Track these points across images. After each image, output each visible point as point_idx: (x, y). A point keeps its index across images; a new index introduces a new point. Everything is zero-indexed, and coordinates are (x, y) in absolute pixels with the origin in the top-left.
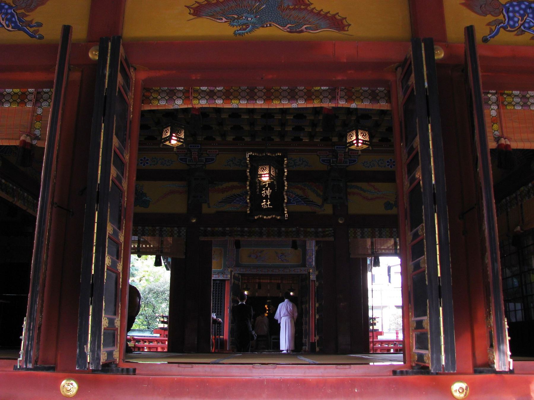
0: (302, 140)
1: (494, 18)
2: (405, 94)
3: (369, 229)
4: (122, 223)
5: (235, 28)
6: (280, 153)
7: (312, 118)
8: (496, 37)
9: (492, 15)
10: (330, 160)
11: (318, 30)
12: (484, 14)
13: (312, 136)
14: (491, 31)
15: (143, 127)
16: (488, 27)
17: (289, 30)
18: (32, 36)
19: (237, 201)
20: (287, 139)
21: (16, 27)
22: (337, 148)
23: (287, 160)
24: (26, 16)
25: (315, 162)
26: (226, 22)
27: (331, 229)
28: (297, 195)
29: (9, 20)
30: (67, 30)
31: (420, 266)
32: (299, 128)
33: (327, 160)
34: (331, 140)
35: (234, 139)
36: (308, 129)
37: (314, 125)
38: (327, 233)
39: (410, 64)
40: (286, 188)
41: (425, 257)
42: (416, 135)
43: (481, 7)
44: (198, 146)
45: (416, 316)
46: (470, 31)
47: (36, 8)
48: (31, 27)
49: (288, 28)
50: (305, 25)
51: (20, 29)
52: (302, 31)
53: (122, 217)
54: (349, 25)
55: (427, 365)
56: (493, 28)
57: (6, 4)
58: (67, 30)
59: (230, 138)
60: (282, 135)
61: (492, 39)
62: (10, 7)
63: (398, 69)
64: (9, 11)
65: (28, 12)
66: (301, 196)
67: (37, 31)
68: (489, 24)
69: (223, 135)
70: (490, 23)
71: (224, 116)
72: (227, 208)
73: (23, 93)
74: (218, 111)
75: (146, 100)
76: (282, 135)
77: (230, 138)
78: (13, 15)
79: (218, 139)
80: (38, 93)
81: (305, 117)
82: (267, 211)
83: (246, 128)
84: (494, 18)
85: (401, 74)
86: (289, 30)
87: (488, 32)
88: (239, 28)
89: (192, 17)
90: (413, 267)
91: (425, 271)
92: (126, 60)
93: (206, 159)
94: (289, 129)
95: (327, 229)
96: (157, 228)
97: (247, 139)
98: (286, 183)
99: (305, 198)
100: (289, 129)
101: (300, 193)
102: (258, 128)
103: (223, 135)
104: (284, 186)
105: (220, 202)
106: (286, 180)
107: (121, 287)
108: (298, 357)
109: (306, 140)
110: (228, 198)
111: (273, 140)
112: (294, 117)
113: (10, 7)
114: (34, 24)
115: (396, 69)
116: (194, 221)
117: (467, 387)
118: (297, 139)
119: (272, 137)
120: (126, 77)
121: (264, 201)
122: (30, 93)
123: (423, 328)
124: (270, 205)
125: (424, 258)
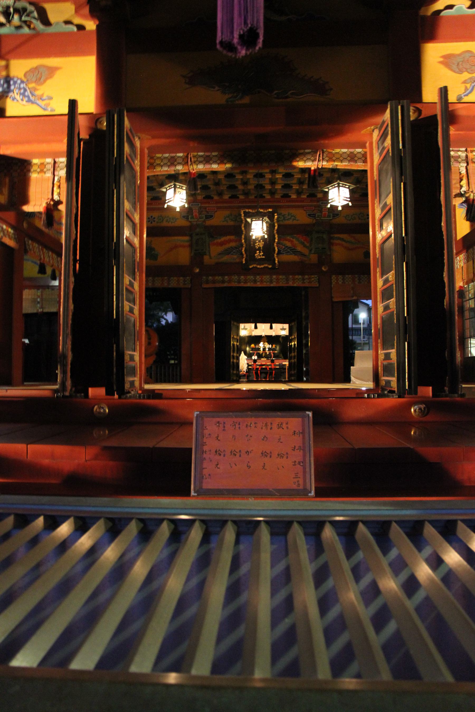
0: (290, 196)
1: (470, 76)
2: (380, 154)
3: (350, 276)
4: (136, 275)
5: (227, 96)
6: (271, 208)
7: (299, 176)
8: (470, 95)
9: (468, 72)
10: (315, 214)
11: (302, 95)
12: (460, 72)
13: (299, 193)
14: (466, 89)
15: (150, 189)
16: (463, 85)
17: (275, 96)
18: (45, 109)
19: (234, 252)
20: (277, 196)
21: (29, 101)
22: (322, 203)
23: (278, 215)
24: (37, 90)
25: (301, 217)
26: (218, 90)
27: (316, 276)
28: (287, 247)
29: (23, 95)
30: (73, 104)
31: (389, 307)
32: (287, 186)
33: (313, 214)
34: (316, 196)
35: (230, 197)
36: (296, 187)
37: (301, 182)
38: (313, 279)
39: (388, 125)
40: (276, 240)
41: (393, 300)
42: (390, 193)
43: (458, 64)
44: (198, 205)
45: (383, 349)
46: (444, 92)
47: (45, 81)
48: (43, 100)
49: (275, 94)
50: (291, 90)
51: (33, 103)
52: (287, 97)
53: (136, 270)
54: (331, 89)
55: (393, 389)
56: (468, 86)
57: (18, 79)
58: (73, 104)
59: (226, 197)
60: (272, 193)
61: (466, 97)
62: (22, 82)
63: (375, 131)
64: (22, 86)
65: (39, 85)
66: (290, 248)
67: (49, 104)
68: (465, 82)
69: (220, 194)
70: (466, 80)
71: (221, 177)
72: (225, 258)
73: (42, 164)
74: (214, 173)
75: (152, 166)
76: (272, 193)
77: (226, 197)
78: (25, 90)
79: (216, 198)
80: (55, 162)
81: (293, 176)
82: (260, 261)
83: (240, 187)
84: (470, 76)
85: (378, 136)
86: (275, 96)
87: (463, 90)
88: (230, 96)
89: (188, 86)
90: (382, 308)
91: (393, 312)
92: (130, 130)
93: (206, 216)
94: (278, 187)
95: (313, 276)
96: (166, 278)
97: (242, 197)
98: (276, 236)
99: (294, 249)
100: (278, 187)
101: (289, 244)
102: (251, 187)
103: (220, 194)
104: (275, 239)
105: (220, 254)
106: (277, 233)
107: (138, 328)
108: (290, 384)
109: (294, 196)
110: (226, 250)
111: (264, 197)
112: (283, 176)
113: (22, 82)
114: (45, 97)
115: (373, 131)
116: (197, 270)
117: (424, 408)
118: (286, 196)
119: (264, 195)
120: (132, 145)
121: (258, 252)
122: (48, 163)
123: (391, 359)
124: (263, 255)
125: (393, 300)
